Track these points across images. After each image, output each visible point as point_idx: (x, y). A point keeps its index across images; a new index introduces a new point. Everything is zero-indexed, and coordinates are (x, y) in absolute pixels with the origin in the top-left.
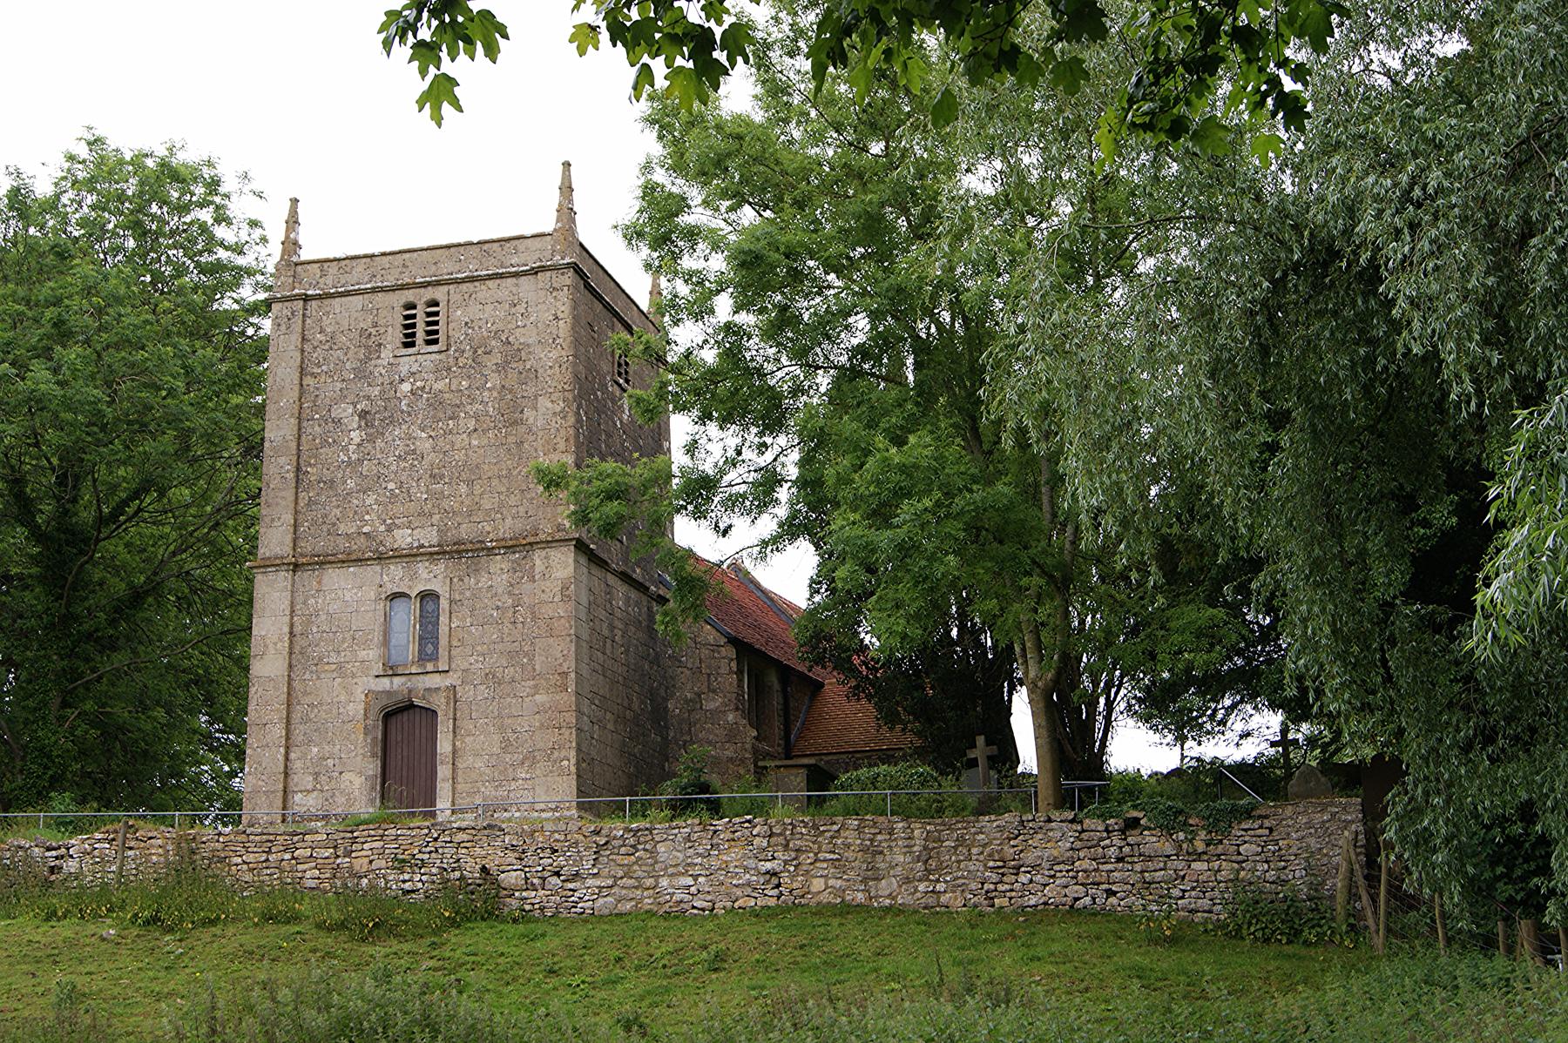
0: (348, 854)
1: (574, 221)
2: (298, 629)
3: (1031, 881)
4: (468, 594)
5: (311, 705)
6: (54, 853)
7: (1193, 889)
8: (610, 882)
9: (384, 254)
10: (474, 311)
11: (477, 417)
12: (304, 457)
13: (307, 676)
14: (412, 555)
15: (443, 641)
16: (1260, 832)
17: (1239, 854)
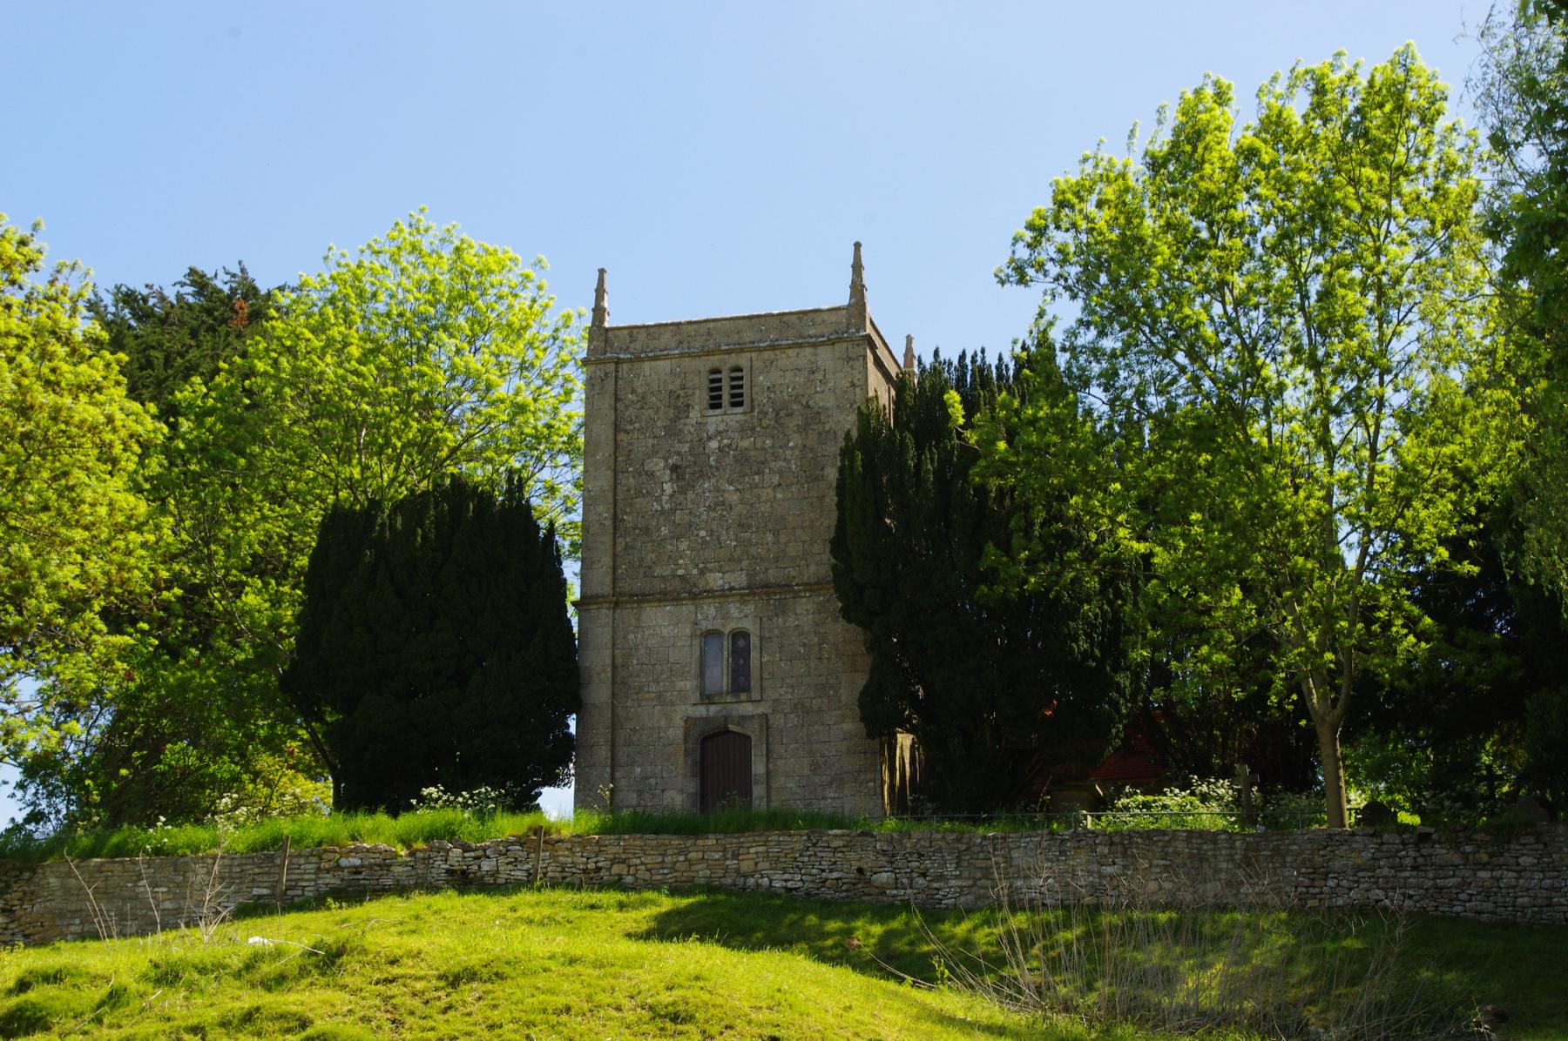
0: (735, 856)
1: (863, 296)
2: (619, 661)
3: (1338, 885)
4: (776, 632)
5: (632, 730)
6: (473, 854)
7: (1479, 893)
8: (971, 882)
9: (690, 323)
10: (775, 376)
11: (780, 473)
12: (620, 505)
13: (629, 703)
14: (725, 594)
15: (755, 674)
16: (1536, 846)
17: (1518, 864)
